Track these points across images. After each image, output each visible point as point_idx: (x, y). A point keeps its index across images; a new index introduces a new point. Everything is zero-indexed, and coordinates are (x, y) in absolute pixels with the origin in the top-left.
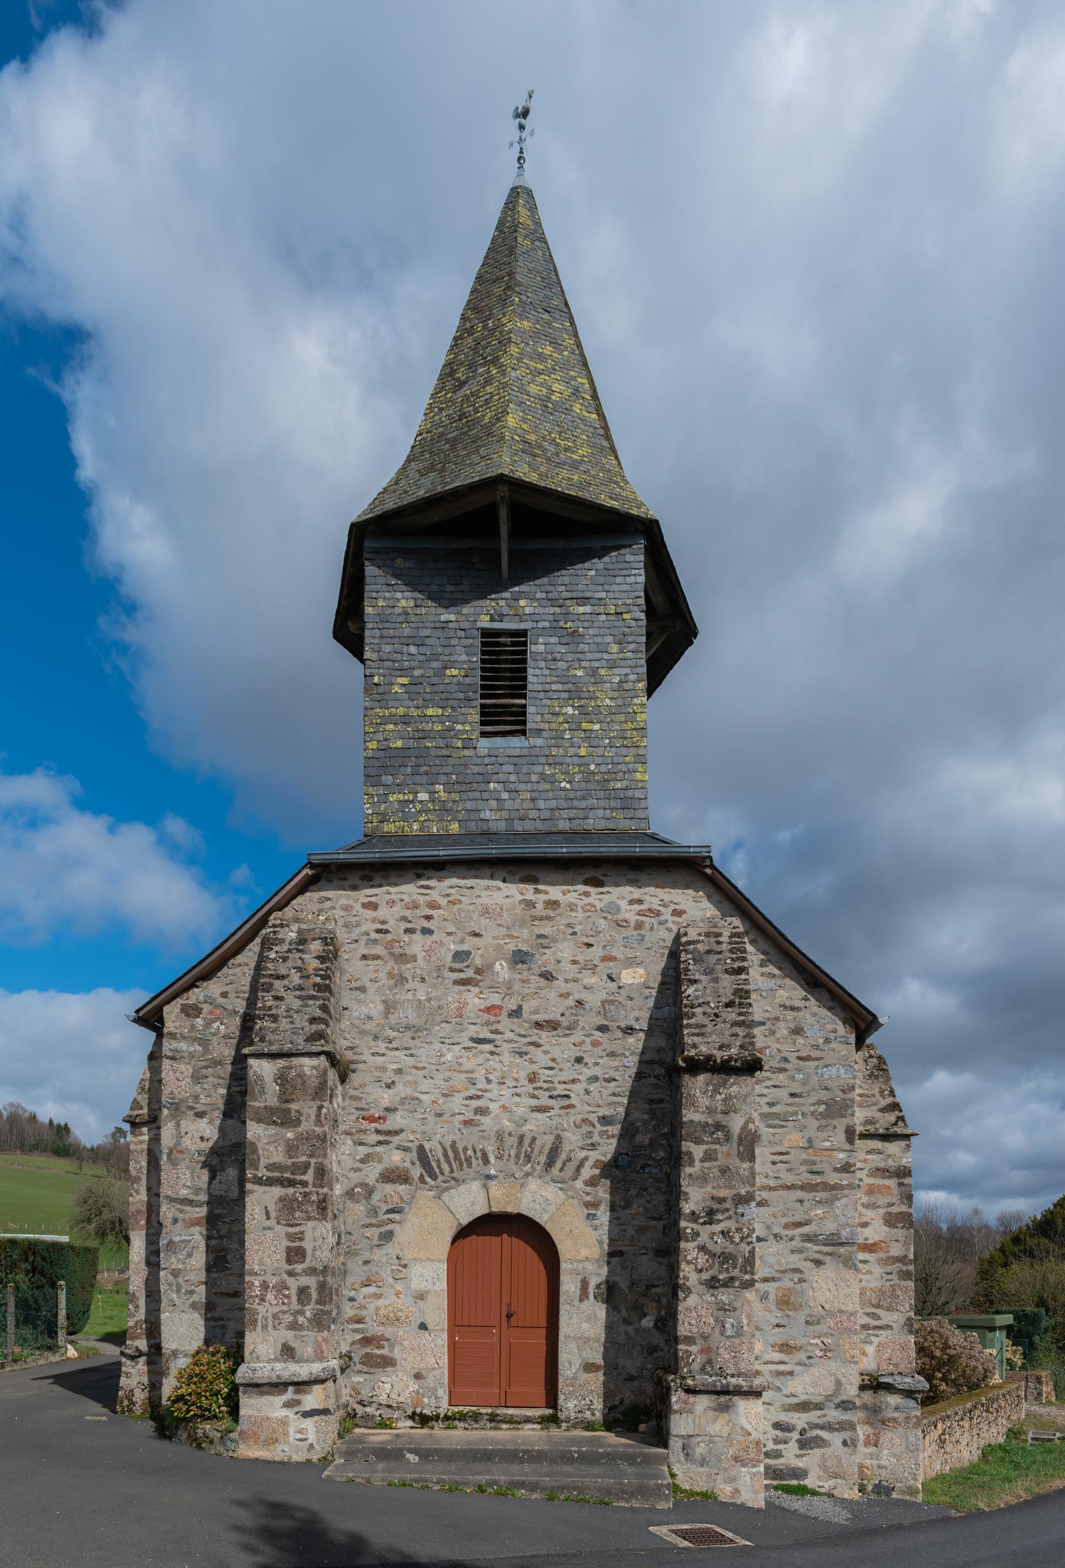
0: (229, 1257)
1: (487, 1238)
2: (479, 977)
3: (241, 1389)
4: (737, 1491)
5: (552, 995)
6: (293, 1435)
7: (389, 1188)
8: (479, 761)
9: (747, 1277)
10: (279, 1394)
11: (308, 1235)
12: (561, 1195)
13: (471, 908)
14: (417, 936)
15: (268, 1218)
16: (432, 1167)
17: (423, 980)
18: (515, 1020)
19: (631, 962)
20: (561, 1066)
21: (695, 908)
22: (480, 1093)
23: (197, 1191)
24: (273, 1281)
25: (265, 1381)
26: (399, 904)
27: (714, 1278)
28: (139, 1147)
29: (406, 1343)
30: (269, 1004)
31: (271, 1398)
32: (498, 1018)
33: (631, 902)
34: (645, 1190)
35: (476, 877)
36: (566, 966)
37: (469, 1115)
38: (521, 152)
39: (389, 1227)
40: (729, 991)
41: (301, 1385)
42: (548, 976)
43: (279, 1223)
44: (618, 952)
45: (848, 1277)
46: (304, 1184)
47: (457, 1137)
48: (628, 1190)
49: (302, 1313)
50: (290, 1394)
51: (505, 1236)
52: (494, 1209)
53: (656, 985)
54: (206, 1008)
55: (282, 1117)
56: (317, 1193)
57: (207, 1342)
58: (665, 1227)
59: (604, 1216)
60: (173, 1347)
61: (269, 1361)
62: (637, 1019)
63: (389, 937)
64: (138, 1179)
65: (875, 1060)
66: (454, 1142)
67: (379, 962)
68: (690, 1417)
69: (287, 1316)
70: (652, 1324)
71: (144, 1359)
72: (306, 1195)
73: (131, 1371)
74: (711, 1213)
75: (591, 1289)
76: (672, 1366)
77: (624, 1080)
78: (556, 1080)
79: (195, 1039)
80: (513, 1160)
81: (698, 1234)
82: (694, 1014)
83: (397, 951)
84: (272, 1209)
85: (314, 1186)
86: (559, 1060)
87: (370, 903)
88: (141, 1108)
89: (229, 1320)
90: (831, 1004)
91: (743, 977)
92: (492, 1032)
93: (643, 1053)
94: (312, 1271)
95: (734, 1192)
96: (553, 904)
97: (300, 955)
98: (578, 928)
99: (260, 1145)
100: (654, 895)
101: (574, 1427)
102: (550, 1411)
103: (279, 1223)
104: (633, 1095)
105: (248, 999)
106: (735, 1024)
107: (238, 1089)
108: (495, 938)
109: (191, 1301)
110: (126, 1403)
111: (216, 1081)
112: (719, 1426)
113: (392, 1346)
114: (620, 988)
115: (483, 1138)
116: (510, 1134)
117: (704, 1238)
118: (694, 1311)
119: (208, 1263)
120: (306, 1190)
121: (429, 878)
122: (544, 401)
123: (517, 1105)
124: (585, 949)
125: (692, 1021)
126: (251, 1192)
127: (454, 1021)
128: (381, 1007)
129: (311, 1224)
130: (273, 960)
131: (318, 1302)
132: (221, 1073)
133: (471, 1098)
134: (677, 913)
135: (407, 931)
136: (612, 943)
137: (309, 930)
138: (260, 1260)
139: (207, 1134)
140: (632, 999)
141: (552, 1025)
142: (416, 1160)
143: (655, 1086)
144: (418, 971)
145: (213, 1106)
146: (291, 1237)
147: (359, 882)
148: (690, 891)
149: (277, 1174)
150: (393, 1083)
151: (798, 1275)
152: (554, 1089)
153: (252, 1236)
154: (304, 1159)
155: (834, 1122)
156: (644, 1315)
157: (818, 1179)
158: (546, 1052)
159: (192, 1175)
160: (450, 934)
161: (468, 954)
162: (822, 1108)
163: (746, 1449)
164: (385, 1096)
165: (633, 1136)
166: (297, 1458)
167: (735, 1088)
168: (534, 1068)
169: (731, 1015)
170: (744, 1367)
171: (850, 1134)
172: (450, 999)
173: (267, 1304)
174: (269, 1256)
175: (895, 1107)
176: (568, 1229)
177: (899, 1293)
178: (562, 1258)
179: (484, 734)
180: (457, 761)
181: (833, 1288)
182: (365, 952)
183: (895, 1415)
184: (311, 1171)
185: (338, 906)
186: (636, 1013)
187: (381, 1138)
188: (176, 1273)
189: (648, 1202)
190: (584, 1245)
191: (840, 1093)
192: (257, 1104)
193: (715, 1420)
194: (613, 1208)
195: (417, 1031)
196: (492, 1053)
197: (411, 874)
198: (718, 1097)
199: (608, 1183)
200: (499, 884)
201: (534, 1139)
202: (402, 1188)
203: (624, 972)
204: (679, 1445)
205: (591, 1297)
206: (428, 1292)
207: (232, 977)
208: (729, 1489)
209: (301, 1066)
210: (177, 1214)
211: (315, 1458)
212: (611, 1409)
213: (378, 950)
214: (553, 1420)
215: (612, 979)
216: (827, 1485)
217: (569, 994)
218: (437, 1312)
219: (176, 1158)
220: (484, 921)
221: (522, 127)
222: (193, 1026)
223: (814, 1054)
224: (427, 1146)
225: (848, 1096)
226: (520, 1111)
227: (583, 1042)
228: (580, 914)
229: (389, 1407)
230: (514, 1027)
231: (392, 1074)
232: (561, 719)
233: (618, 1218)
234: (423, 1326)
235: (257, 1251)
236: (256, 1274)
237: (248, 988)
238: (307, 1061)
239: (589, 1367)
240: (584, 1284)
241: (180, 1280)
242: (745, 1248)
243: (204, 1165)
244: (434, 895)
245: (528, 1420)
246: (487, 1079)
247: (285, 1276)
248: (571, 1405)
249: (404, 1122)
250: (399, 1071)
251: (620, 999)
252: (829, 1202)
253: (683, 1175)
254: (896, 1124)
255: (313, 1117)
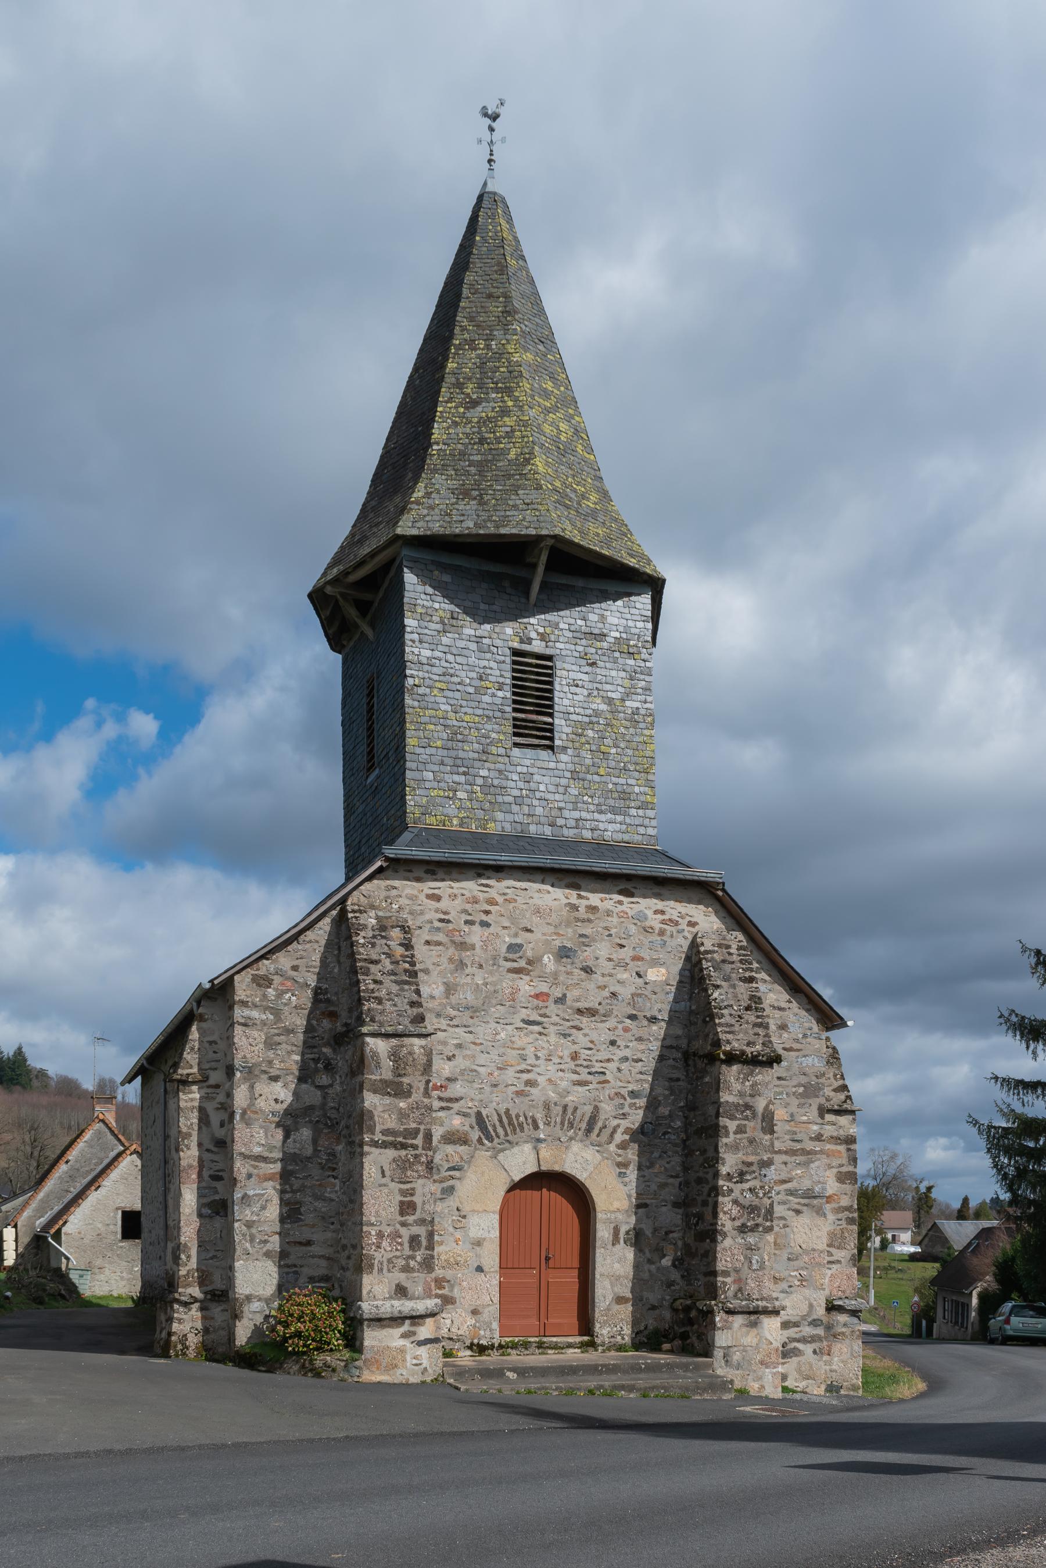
0: (302, 1210)
1: (529, 1192)
2: (530, 968)
3: (366, 1323)
4: (763, 1387)
5: (591, 986)
6: (410, 1361)
7: (450, 1149)
8: (512, 768)
9: (768, 1224)
10: (397, 1327)
11: (419, 1191)
12: (598, 1157)
13: (524, 906)
14: (476, 928)
15: (384, 1176)
16: (491, 1131)
17: (481, 966)
18: (560, 1006)
19: (655, 963)
20: (598, 1047)
21: (706, 921)
22: (530, 1068)
23: (271, 1148)
24: (387, 1230)
25: (388, 1316)
26: (460, 898)
27: (744, 1225)
28: (189, 1104)
29: (464, 1284)
30: (371, 986)
31: (390, 1331)
32: (546, 1004)
33: (656, 912)
34: (665, 1153)
35: (529, 881)
36: (602, 962)
37: (521, 1087)
38: (491, 155)
39: (451, 1183)
40: (746, 997)
41: (416, 1319)
42: (588, 970)
43: (392, 1180)
44: (645, 954)
45: (819, 1223)
46: (415, 1147)
47: (510, 1105)
48: (652, 1153)
49: (413, 1258)
50: (406, 1327)
51: (544, 1190)
52: (543, 1168)
53: (675, 983)
54: (277, 980)
55: (396, 1089)
56: (426, 1155)
57: (280, 1288)
58: (680, 1184)
59: (632, 1174)
60: (247, 1292)
61: (384, 1299)
62: (660, 1011)
63: (451, 926)
64: (190, 1135)
65: (830, 1050)
66: (508, 1110)
67: (441, 948)
68: (730, 1334)
69: (400, 1260)
70: (670, 1263)
71: (197, 1305)
72: (416, 1156)
73: (184, 1317)
74: (742, 1174)
75: (622, 1235)
76: (712, 1292)
77: (649, 1061)
78: (594, 1059)
79: (266, 1008)
80: (558, 1126)
81: (732, 1191)
82: (723, 1016)
83: (458, 939)
84: (386, 1168)
85: (424, 1149)
86: (596, 1042)
87: (433, 895)
88: (191, 1067)
89: (301, 1266)
90: (808, 1007)
91: (754, 985)
92: (541, 1015)
93: (664, 1039)
94: (422, 1222)
95: (758, 1158)
96: (593, 909)
97: (384, 941)
98: (613, 931)
99: (376, 1113)
100: (674, 908)
101: (609, 1349)
102: (586, 1338)
103: (392, 1180)
104: (656, 1073)
105: (319, 974)
106: (756, 1025)
107: (312, 1056)
108: (544, 934)
109: (265, 1249)
110: (180, 1347)
111: (289, 1048)
112: (750, 1339)
113: (452, 1287)
114: (646, 983)
115: (533, 1106)
116: (556, 1104)
117: (736, 1194)
118: (729, 1251)
119: (281, 1215)
120: (417, 1152)
121: (489, 878)
122: (556, 441)
123: (561, 1079)
124: (618, 948)
125: (722, 1020)
126: (368, 1153)
127: (508, 1004)
128: (442, 988)
129: (420, 1181)
130: (363, 945)
131: (427, 1248)
132: (294, 1040)
133: (522, 1072)
134: (692, 924)
135: (466, 922)
136: (641, 945)
137: (386, 918)
138: (377, 1212)
139: (282, 1097)
140: (655, 993)
141: (591, 1012)
142: (474, 1124)
143: (674, 1067)
144: (477, 959)
145: (288, 1072)
146: (403, 1193)
147: (423, 875)
148: (701, 907)
149: (391, 1138)
150: (454, 1056)
151: (783, 1222)
152: (593, 1066)
153: (369, 1192)
154: (414, 1125)
155: (810, 1101)
156: (664, 1256)
157: (798, 1146)
158: (585, 1035)
159: (266, 1134)
160: (504, 928)
161: (520, 946)
162: (801, 1090)
163: (769, 1355)
164: (447, 1067)
165: (656, 1108)
166: (414, 1380)
167: (760, 1077)
168: (576, 1048)
169: (750, 1017)
170: (765, 1293)
171: (823, 1111)
172: (504, 985)
173: (382, 1250)
174: (384, 1209)
175: (844, 1088)
176: (603, 1185)
177: (846, 1235)
178: (598, 1209)
179: (516, 745)
180: (492, 766)
181: (808, 1232)
182: (428, 938)
183: (844, 1330)
184: (420, 1136)
185: (403, 895)
186: (659, 1006)
187: (444, 1104)
188: (249, 1225)
189: (668, 1163)
190: (614, 1197)
191: (814, 1078)
192: (373, 1077)
193: (748, 1333)
194: (639, 1169)
195: (475, 1012)
196: (540, 1034)
197: (472, 873)
198: (747, 1083)
199: (636, 1146)
200: (549, 888)
201: (576, 1109)
202: (462, 1149)
203: (650, 970)
204: (721, 1354)
205: (622, 1241)
206: (484, 1239)
207: (302, 953)
208: (756, 1386)
209: (412, 1045)
210: (251, 1170)
211: (428, 1379)
212: (637, 1333)
213: (440, 937)
214: (592, 1344)
215: (639, 975)
216: (802, 1385)
217: (605, 987)
218: (490, 1257)
219: (250, 1118)
220: (536, 919)
221: (492, 129)
222: (265, 996)
223: (795, 1046)
224: (484, 1113)
225: (820, 1081)
226: (564, 1084)
227: (616, 1028)
228: (615, 920)
229: (451, 1339)
230: (560, 1012)
231: (453, 1048)
232: (583, 740)
233: (644, 1176)
234: (480, 1269)
235: (374, 1205)
236: (373, 1225)
237: (318, 964)
238: (416, 1041)
239: (620, 1300)
240: (616, 1231)
241: (254, 1231)
242: (767, 1202)
243: (278, 1125)
244: (493, 893)
245: (570, 1346)
246: (536, 1056)
247: (398, 1226)
248: (605, 1332)
249: (464, 1091)
250: (459, 1046)
251: (646, 993)
252: (806, 1164)
253: (720, 1144)
254: (845, 1102)
255: (422, 1090)
